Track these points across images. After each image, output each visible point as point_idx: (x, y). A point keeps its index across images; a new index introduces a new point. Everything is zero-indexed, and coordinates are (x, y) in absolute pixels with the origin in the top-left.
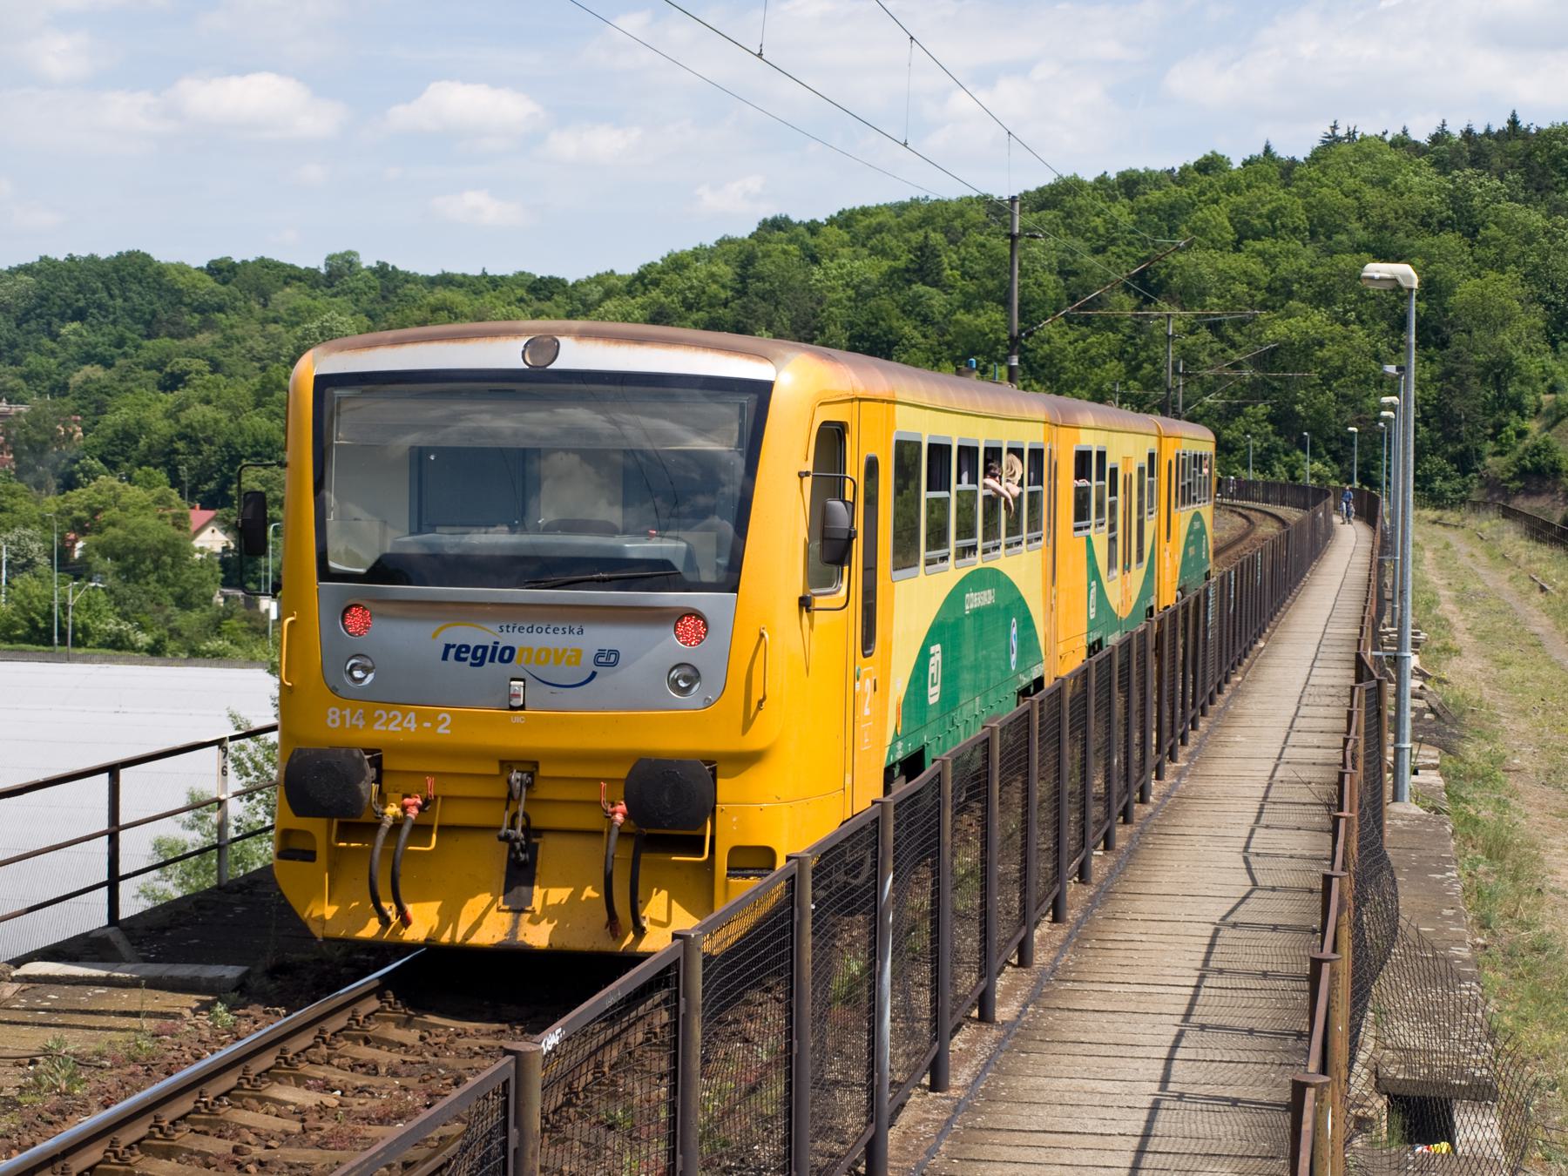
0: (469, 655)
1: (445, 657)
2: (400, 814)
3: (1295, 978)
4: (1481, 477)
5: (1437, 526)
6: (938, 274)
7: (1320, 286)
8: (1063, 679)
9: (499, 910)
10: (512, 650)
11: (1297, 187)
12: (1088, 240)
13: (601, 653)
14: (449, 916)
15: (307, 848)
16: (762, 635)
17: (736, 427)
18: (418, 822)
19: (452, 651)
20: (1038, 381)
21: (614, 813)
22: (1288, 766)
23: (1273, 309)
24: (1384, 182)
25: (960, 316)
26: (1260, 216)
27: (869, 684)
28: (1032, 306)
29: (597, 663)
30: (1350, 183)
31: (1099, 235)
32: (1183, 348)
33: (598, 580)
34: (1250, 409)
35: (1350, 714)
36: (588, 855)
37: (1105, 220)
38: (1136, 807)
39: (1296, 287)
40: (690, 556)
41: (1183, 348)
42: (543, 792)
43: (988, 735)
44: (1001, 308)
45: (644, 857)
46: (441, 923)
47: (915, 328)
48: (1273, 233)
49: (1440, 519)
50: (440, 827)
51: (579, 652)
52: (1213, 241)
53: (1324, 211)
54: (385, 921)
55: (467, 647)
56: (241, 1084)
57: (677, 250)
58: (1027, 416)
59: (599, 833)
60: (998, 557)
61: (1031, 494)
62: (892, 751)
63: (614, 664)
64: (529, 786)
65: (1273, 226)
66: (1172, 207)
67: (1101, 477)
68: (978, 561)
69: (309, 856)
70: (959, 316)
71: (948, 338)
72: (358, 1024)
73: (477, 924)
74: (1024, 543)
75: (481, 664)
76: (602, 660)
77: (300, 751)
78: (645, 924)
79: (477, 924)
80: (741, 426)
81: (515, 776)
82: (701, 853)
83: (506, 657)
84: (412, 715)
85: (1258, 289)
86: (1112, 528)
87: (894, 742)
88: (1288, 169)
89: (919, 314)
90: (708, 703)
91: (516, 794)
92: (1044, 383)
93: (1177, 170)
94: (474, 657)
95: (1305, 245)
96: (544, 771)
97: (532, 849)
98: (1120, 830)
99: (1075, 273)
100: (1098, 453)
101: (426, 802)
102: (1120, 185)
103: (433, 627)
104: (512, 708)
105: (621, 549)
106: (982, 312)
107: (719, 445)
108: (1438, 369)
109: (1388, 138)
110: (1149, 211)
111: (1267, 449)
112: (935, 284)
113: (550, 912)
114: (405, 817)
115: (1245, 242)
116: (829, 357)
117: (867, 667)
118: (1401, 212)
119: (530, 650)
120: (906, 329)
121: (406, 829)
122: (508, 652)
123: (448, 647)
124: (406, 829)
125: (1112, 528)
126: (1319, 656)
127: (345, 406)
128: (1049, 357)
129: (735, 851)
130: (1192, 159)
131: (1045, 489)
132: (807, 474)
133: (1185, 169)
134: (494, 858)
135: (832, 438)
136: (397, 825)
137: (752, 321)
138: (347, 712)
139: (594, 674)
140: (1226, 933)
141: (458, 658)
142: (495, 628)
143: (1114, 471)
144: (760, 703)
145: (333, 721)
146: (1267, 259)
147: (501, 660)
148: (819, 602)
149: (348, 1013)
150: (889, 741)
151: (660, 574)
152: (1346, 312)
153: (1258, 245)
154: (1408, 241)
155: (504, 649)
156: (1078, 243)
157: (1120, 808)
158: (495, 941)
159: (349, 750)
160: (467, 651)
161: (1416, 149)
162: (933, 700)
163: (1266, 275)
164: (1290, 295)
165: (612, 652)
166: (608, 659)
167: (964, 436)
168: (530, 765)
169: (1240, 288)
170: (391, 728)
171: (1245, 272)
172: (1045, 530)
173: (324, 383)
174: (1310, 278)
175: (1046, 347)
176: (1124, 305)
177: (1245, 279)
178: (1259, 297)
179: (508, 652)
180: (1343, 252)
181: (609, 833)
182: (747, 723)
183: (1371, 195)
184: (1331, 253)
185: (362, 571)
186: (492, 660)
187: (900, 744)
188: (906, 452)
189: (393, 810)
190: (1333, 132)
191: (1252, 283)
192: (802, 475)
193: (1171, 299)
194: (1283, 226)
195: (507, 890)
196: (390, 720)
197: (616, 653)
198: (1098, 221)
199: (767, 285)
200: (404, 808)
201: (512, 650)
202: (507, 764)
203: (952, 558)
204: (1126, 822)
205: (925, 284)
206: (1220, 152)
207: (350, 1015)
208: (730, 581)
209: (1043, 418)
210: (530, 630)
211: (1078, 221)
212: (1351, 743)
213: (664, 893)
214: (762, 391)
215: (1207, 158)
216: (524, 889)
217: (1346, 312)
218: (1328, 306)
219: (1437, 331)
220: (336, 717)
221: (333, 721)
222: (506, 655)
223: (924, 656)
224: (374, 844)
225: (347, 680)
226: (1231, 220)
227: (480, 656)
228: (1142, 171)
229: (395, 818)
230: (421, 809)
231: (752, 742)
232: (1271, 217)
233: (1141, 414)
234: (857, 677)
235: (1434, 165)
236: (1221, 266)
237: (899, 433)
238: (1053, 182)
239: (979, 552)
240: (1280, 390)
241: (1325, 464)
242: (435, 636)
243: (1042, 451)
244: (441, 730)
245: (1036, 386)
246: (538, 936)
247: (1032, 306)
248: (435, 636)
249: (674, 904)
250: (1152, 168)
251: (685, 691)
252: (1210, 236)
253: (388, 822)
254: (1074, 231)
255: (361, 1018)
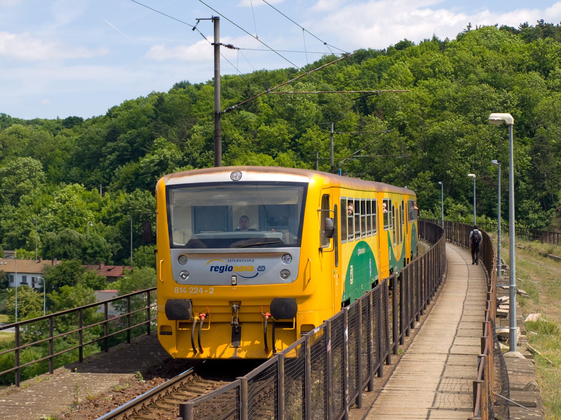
0: (219, 269)
1: (211, 270)
2: (199, 319)
3: (469, 393)
4: (557, 211)
5: (548, 260)
6: (255, 105)
7: (460, 103)
8: (328, 322)
9: (230, 347)
10: (232, 267)
11: (448, 51)
12: (335, 84)
13: (259, 267)
14: (213, 351)
15: (168, 331)
16: (309, 260)
17: (297, 197)
18: (205, 322)
19: (213, 268)
20: (305, 161)
21: (265, 316)
22: (459, 338)
23: (435, 116)
24: (495, 48)
25: (263, 127)
26: (427, 67)
27: (337, 275)
28: (302, 121)
29: (258, 270)
30: (477, 49)
31: (341, 82)
32: (383, 140)
33: (257, 245)
34: (421, 174)
35: (483, 341)
36: (258, 330)
37: (344, 74)
38: (364, 395)
39: (447, 104)
40: (284, 237)
41: (383, 140)
42: (243, 310)
43: (343, 312)
44: (286, 122)
45: (276, 329)
46: (210, 354)
47: (241, 134)
48: (434, 76)
49: (550, 252)
50: (211, 323)
51: (253, 267)
52: (401, 81)
53: (462, 64)
54: (195, 352)
55: (218, 267)
56: (133, 414)
57: (129, 99)
58: (371, 190)
59: (261, 323)
60: (365, 238)
61: (373, 216)
62: (343, 298)
63: (264, 270)
64: (238, 308)
65: (434, 72)
66: (380, 65)
67: (390, 210)
68: (360, 239)
69: (170, 333)
70: (263, 127)
71: (257, 140)
72: (136, 413)
73: (223, 353)
74: (366, 234)
75: (222, 272)
76: (260, 269)
77: (170, 300)
78: (276, 349)
79: (223, 353)
80: (299, 196)
81: (235, 306)
82: (292, 327)
83: (230, 269)
84: (201, 288)
85: (426, 106)
86: (394, 228)
87: (343, 295)
88: (443, 46)
89: (244, 127)
90: (293, 281)
91: (235, 311)
92: (308, 162)
93: (386, 49)
94: (220, 270)
95: (452, 82)
96: (243, 304)
97: (239, 328)
98: (365, 396)
99: (326, 102)
100: (367, 201)
101: (207, 315)
102: (355, 57)
103: (207, 261)
104: (233, 285)
105: (264, 235)
106: (275, 124)
107: (294, 201)
108: (528, 148)
109: (499, 27)
110: (369, 69)
111: (432, 197)
112: (254, 111)
113: (245, 349)
114: (201, 319)
115: (419, 81)
116: (323, 174)
117: (336, 270)
118: (505, 63)
119: (238, 267)
120: (235, 135)
121: (202, 323)
122: (231, 268)
123: (212, 267)
124: (202, 323)
125: (394, 228)
126: (465, 313)
127: (175, 194)
128: (312, 148)
129: (303, 326)
130: (394, 42)
131: (376, 214)
132: (320, 210)
133: (390, 48)
134: (227, 332)
135: (326, 199)
136: (198, 323)
137: (158, 134)
138: (181, 288)
139: (258, 274)
140: (433, 412)
141: (215, 270)
142: (226, 261)
143: (393, 207)
144: (309, 280)
145: (177, 291)
146: (432, 90)
147: (229, 270)
148: (324, 250)
149: (150, 400)
150: (342, 295)
151: (278, 243)
152: (475, 117)
153: (426, 82)
154: (509, 78)
155: (229, 267)
156: (330, 87)
157: (385, 358)
158: (230, 357)
159: (185, 300)
160: (218, 268)
161: (512, 30)
162: (352, 283)
163: (430, 98)
164: (445, 108)
165: (263, 267)
166: (262, 269)
167: (350, 198)
168: (239, 302)
169: (415, 106)
170: (195, 292)
171: (418, 97)
172: (377, 229)
173: (169, 188)
174: (455, 99)
175: (309, 142)
176: (354, 118)
177: (419, 101)
178: (427, 111)
179: (231, 268)
180: (473, 84)
181: (264, 323)
182: (305, 287)
183: (489, 54)
184: (465, 84)
185: (184, 245)
186: (226, 270)
187: (344, 296)
188: (343, 201)
189: (196, 318)
190: (469, 29)
191: (422, 103)
192: (318, 211)
193: (378, 114)
194: (440, 72)
195: (232, 341)
196: (194, 290)
197: (264, 267)
198: (341, 75)
199: (168, 115)
200: (200, 317)
201: (232, 267)
202: (231, 302)
203: (354, 237)
204: (387, 364)
205: (247, 110)
206: (409, 40)
207: (124, 415)
208: (298, 244)
209: (374, 190)
210: (237, 261)
211: (331, 76)
212: (488, 313)
213: (280, 341)
214: (305, 186)
215: (401, 42)
216: (238, 342)
217: (475, 117)
218: (465, 114)
219: (527, 127)
220: (178, 290)
221: (177, 291)
222: (230, 269)
223: (349, 269)
224: (192, 328)
225: (180, 278)
226: (412, 70)
227: (222, 269)
228: (367, 50)
229: (198, 320)
230: (205, 317)
231: (306, 293)
232: (432, 67)
233: (367, 181)
234: (334, 273)
235: (523, 38)
236: (404, 94)
237: (342, 197)
238: (321, 58)
239: (361, 236)
240: (439, 163)
241: (465, 205)
242: (208, 264)
243: (375, 201)
244: (211, 293)
245: (303, 163)
246: (242, 355)
247: (302, 121)
248: (208, 264)
249: (283, 343)
250: (372, 48)
251: (285, 278)
252: (399, 78)
253: (196, 321)
254: (329, 81)
255: (128, 416)
